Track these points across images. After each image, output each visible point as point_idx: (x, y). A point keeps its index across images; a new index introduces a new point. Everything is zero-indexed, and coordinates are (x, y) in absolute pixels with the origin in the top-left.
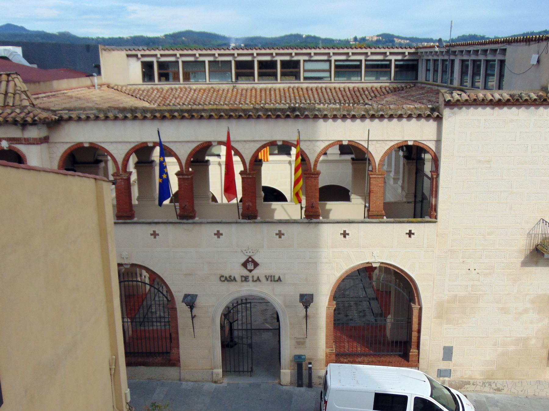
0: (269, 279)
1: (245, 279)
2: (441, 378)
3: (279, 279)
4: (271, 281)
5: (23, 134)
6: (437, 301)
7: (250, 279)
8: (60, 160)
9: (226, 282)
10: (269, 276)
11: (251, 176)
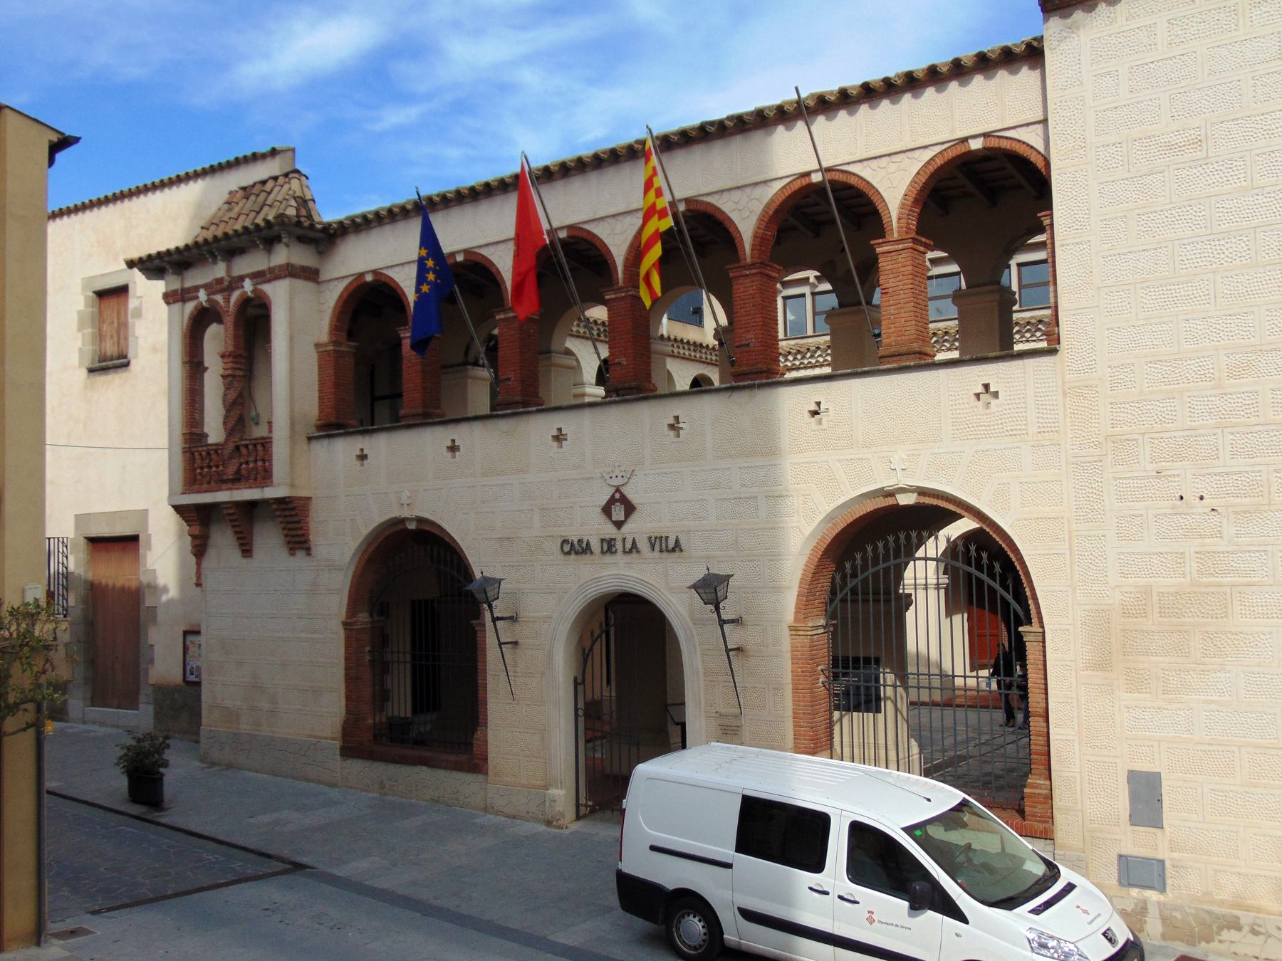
0: (657, 547)
1: (609, 546)
2: (1134, 892)
3: (677, 547)
4: (661, 551)
5: (269, 261)
6: (1088, 607)
7: (619, 546)
8: (333, 314)
9: (573, 556)
10: (656, 538)
11: (623, 295)
